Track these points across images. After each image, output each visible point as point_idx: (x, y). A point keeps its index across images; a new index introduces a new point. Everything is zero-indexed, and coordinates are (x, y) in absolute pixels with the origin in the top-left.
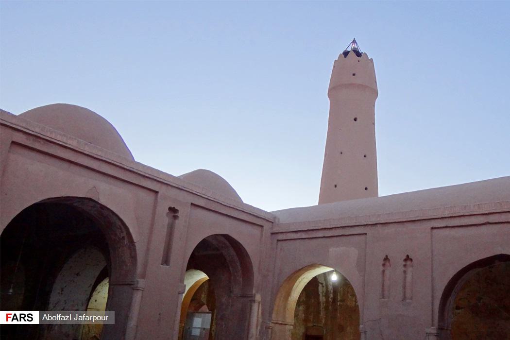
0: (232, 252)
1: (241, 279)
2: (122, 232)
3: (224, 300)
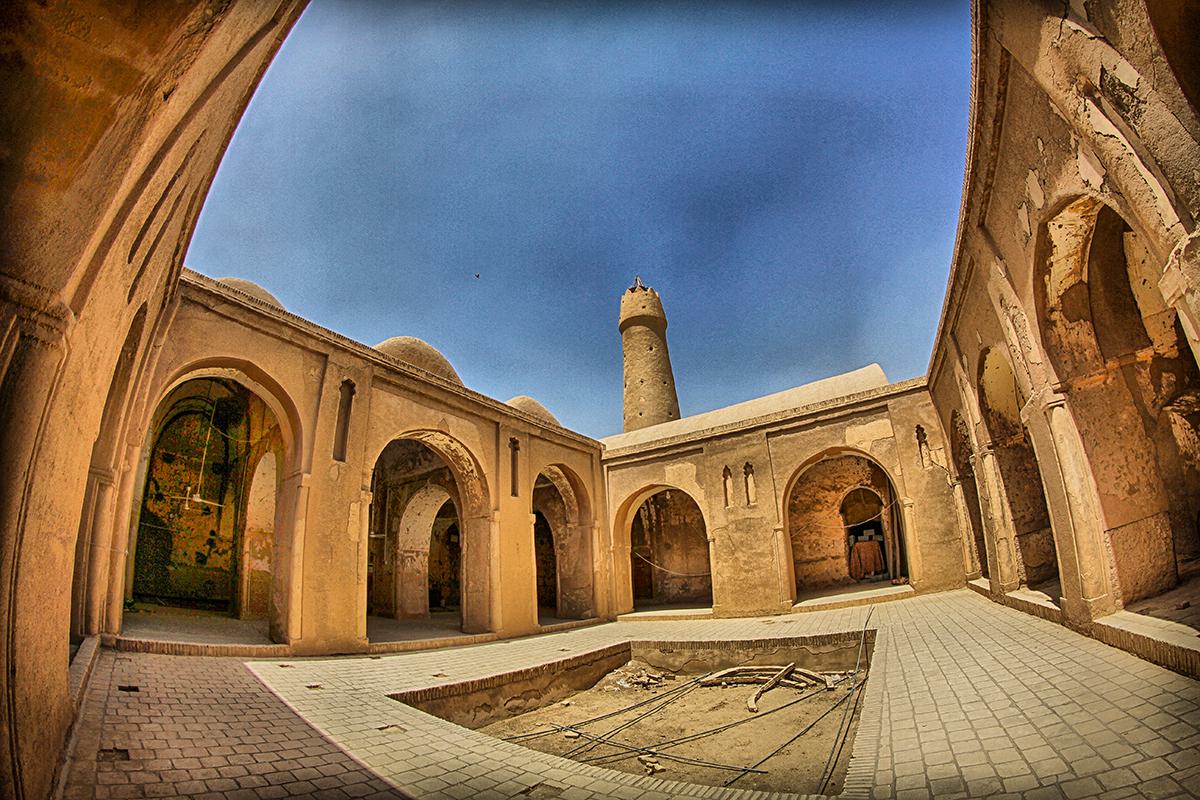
0: (565, 481)
1: (577, 509)
2: (470, 465)
3: (560, 530)
